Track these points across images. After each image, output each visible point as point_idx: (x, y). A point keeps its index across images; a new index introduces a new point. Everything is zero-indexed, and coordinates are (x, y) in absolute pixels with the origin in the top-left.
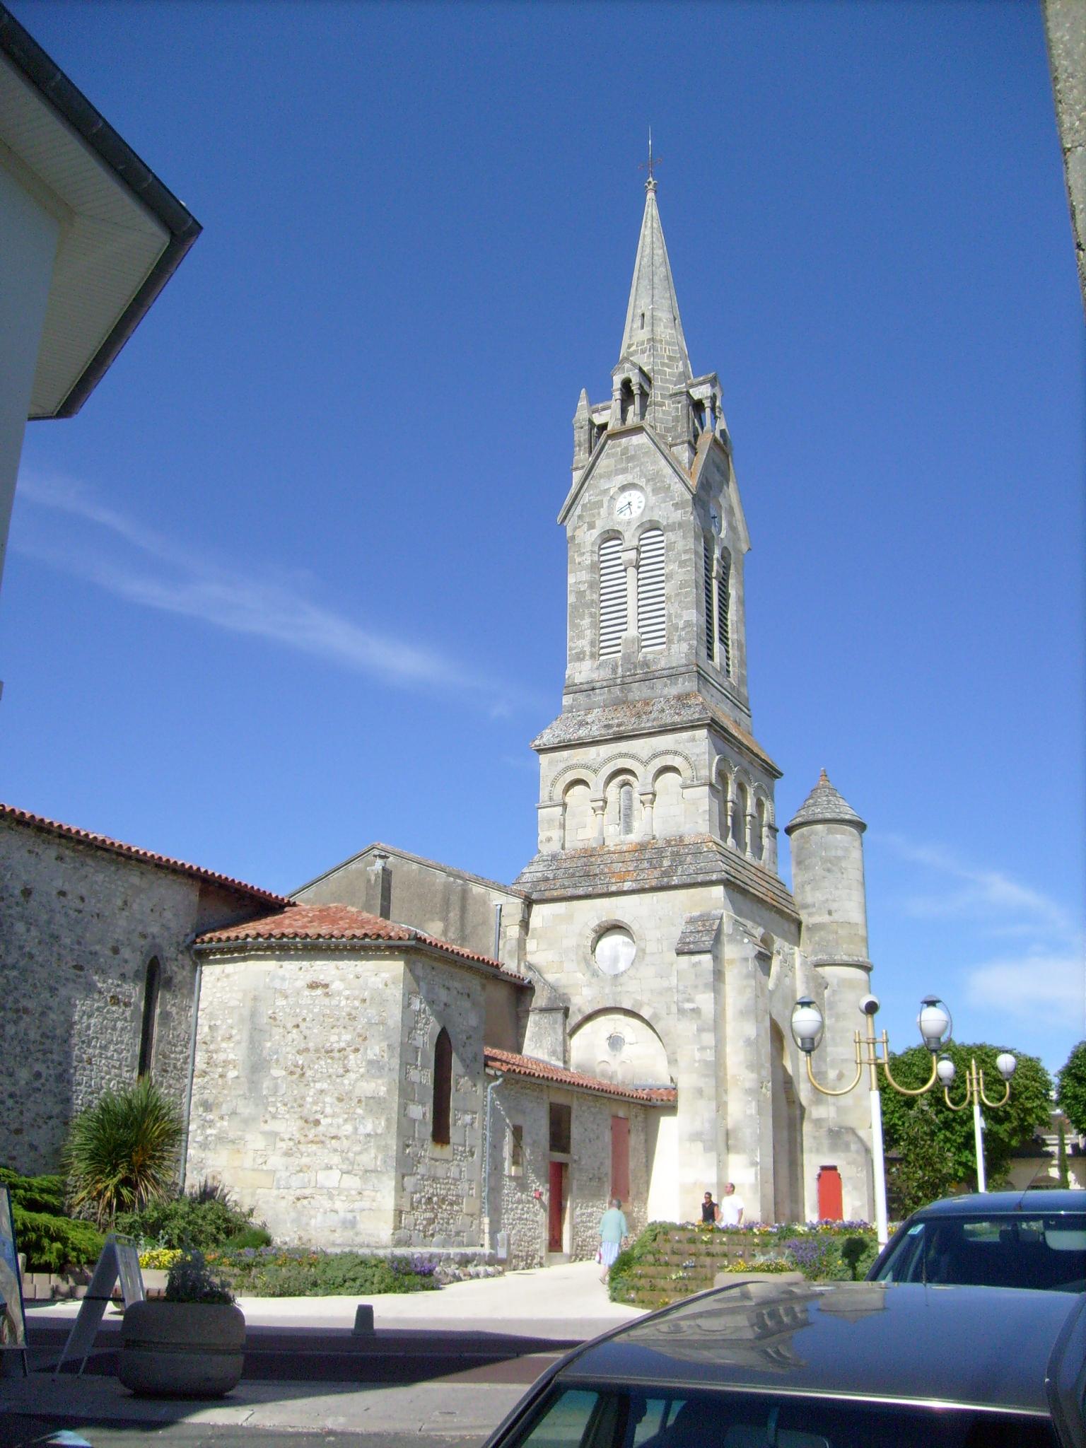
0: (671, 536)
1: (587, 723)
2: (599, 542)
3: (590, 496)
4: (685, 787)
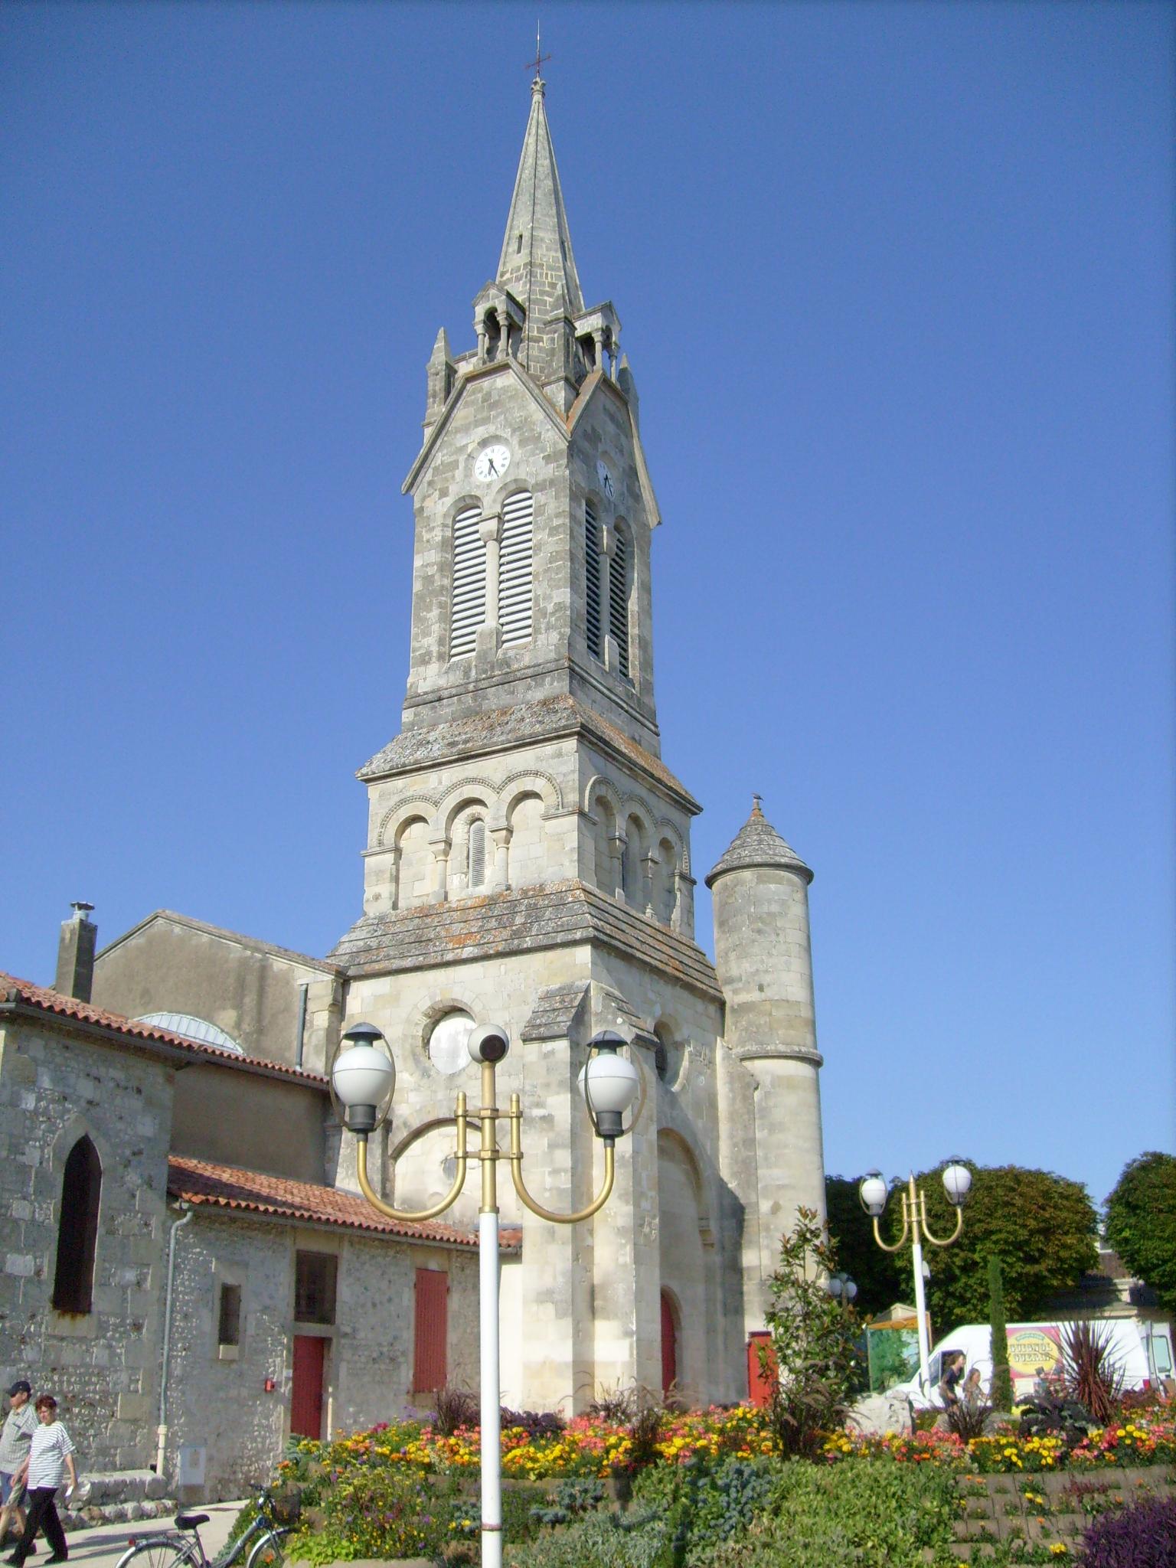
0: (540, 497)
1: (428, 742)
2: (453, 512)
3: (443, 456)
4: (547, 818)
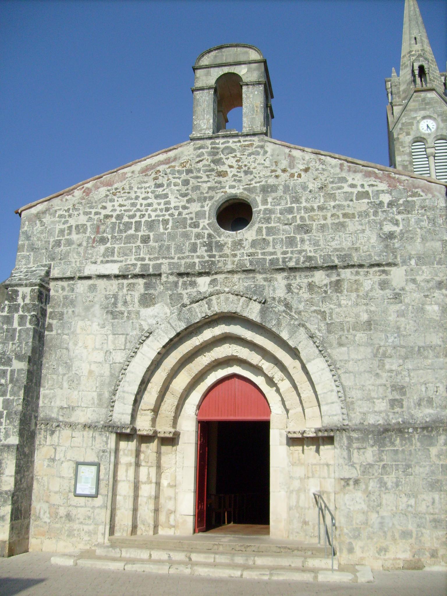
2: (412, 142)
